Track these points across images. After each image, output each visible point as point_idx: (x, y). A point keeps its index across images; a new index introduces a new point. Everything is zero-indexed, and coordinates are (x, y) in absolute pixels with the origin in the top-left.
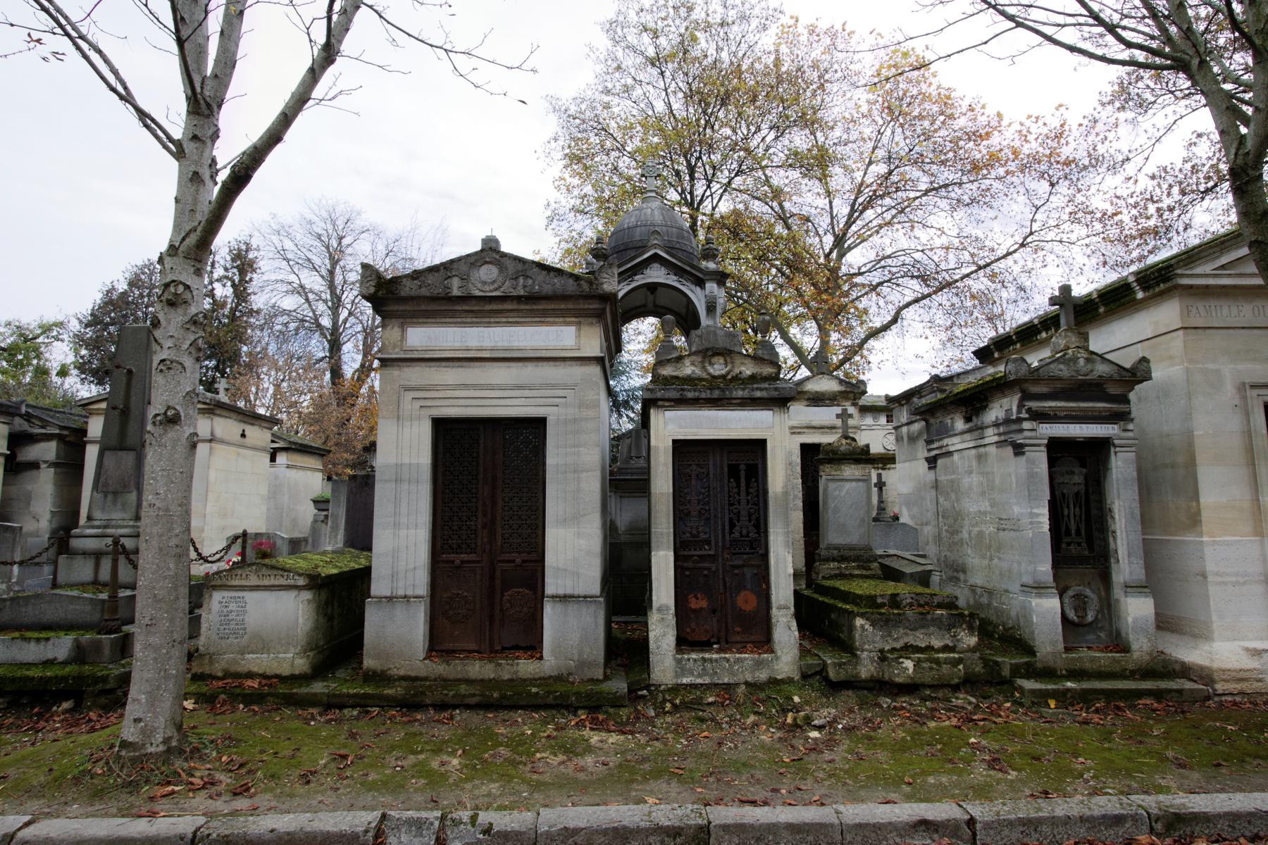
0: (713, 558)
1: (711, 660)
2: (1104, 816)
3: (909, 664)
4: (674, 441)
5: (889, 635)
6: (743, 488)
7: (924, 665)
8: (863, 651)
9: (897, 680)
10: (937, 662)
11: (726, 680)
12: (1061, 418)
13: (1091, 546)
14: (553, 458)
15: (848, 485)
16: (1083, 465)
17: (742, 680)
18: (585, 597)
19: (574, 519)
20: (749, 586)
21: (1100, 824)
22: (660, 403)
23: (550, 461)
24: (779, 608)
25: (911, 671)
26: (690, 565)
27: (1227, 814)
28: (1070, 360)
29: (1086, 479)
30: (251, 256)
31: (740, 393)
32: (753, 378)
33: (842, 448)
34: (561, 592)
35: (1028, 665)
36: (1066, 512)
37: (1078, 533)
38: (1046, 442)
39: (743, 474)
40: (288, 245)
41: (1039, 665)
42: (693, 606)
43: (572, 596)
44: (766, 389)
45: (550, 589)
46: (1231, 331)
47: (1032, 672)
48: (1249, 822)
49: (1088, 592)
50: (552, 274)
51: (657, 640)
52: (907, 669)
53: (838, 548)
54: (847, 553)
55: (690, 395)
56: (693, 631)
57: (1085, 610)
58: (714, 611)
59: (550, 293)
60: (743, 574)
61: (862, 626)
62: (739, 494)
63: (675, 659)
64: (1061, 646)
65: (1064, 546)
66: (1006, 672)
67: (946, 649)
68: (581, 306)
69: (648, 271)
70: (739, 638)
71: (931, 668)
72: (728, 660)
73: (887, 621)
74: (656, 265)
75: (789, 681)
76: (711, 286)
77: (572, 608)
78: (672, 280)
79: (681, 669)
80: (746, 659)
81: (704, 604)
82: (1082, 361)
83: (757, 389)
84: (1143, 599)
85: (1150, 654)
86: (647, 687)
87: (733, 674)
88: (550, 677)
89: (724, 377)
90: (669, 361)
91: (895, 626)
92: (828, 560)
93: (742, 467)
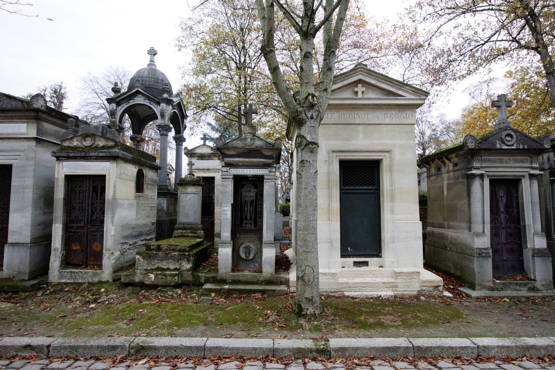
0: (83, 227)
1: (74, 272)
2: (108, 346)
3: (152, 276)
4: (66, 176)
5: (151, 263)
6: (99, 196)
7: (159, 276)
8: (137, 270)
9: (146, 283)
10: (166, 275)
11: (80, 281)
12: (240, 166)
13: (255, 226)
14: (15, 183)
15: (190, 196)
16: (256, 188)
17: (87, 281)
18: (23, 244)
19: (20, 210)
20: (98, 240)
21: (106, 349)
22: (60, 158)
23: (13, 184)
24: (106, 250)
25: (153, 279)
26: (73, 230)
27: (165, 347)
28: (243, 139)
29: (256, 194)
30: (62, 91)
31: (93, 154)
32: (103, 147)
33: (188, 179)
34: (14, 241)
35: (214, 277)
36: (246, 209)
37: (251, 219)
38: (232, 177)
39: (99, 190)
40: (96, 86)
41: (219, 278)
42: (74, 248)
43: (18, 243)
44: (105, 152)
45: (10, 240)
46: (328, 126)
47: (215, 280)
48: (175, 351)
49: (252, 245)
50: (12, 100)
51: (52, 263)
52: (151, 278)
53: (183, 224)
54: (186, 226)
55: (71, 155)
56: (73, 259)
57: (249, 253)
58: (82, 251)
59: (10, 108)
60: (96, 235)
61: (139, 259)
62: (97, 199)
63: (59, 271)
64: (229, 270)
65: (243, 224)
66: (202, 280)
67: (176, 269)
68: (27, 115)
69: (136, 98)
70: (92, 263)
71: (162, 278)
72: (81, 272)
73: (150, 256)
74: (140, 96)
75: (107, 282)
76: (163, 105)
77: (16, 249)
78: (147, 103)
79: (61, 276)
80: (89, 272)
81: (78, 248)
82: (249, 140)
83: (101, 152)
84: (270, 249)
85: (271, 274)
86: (47, 284)
87: (83, 279)
88: (6, 278)
89: (90, 147)
90: (67, 139)
91: (154, 259)
92: (178, 229)
93: (99, 187)
